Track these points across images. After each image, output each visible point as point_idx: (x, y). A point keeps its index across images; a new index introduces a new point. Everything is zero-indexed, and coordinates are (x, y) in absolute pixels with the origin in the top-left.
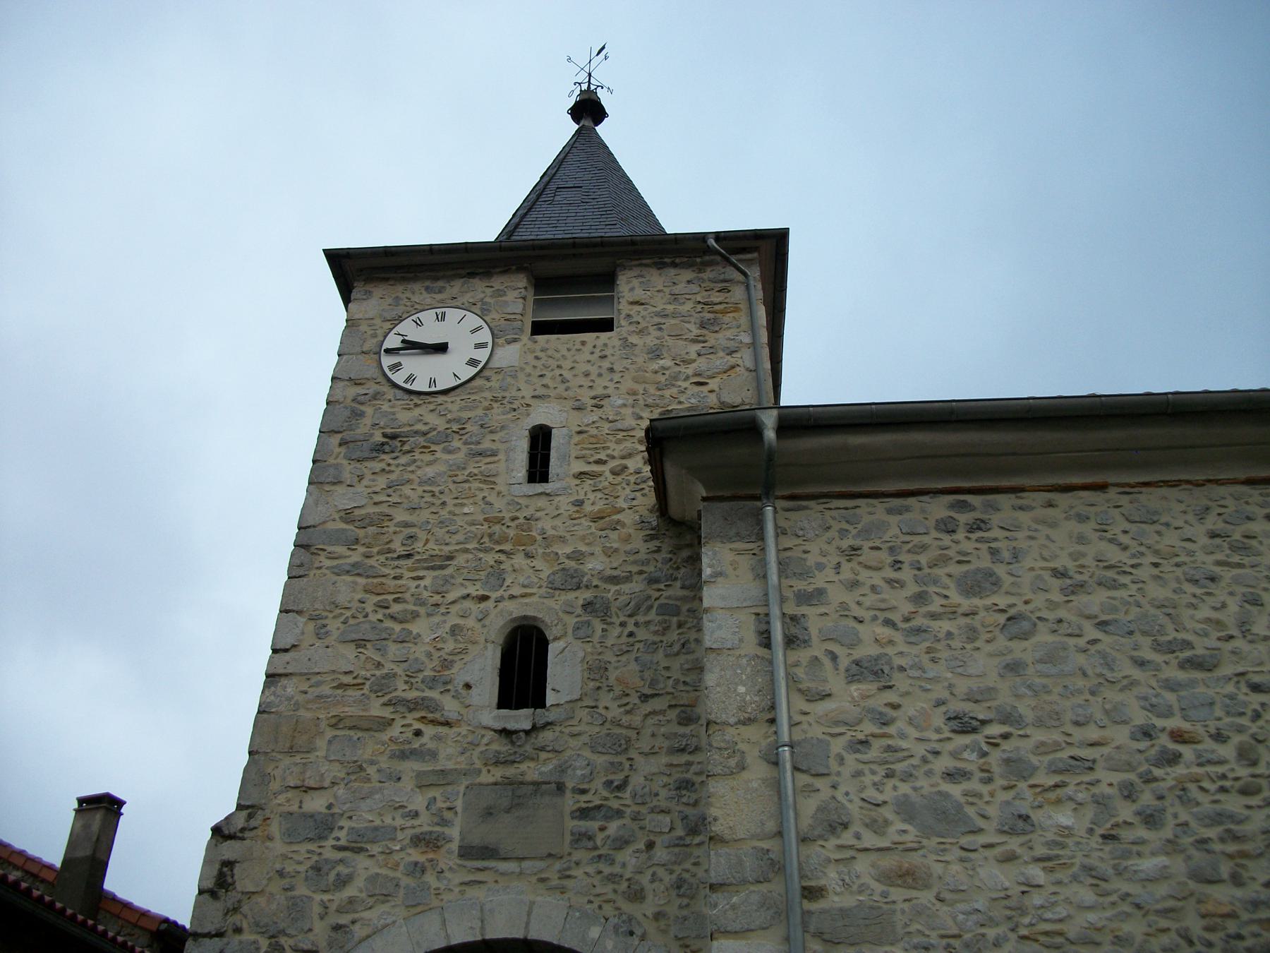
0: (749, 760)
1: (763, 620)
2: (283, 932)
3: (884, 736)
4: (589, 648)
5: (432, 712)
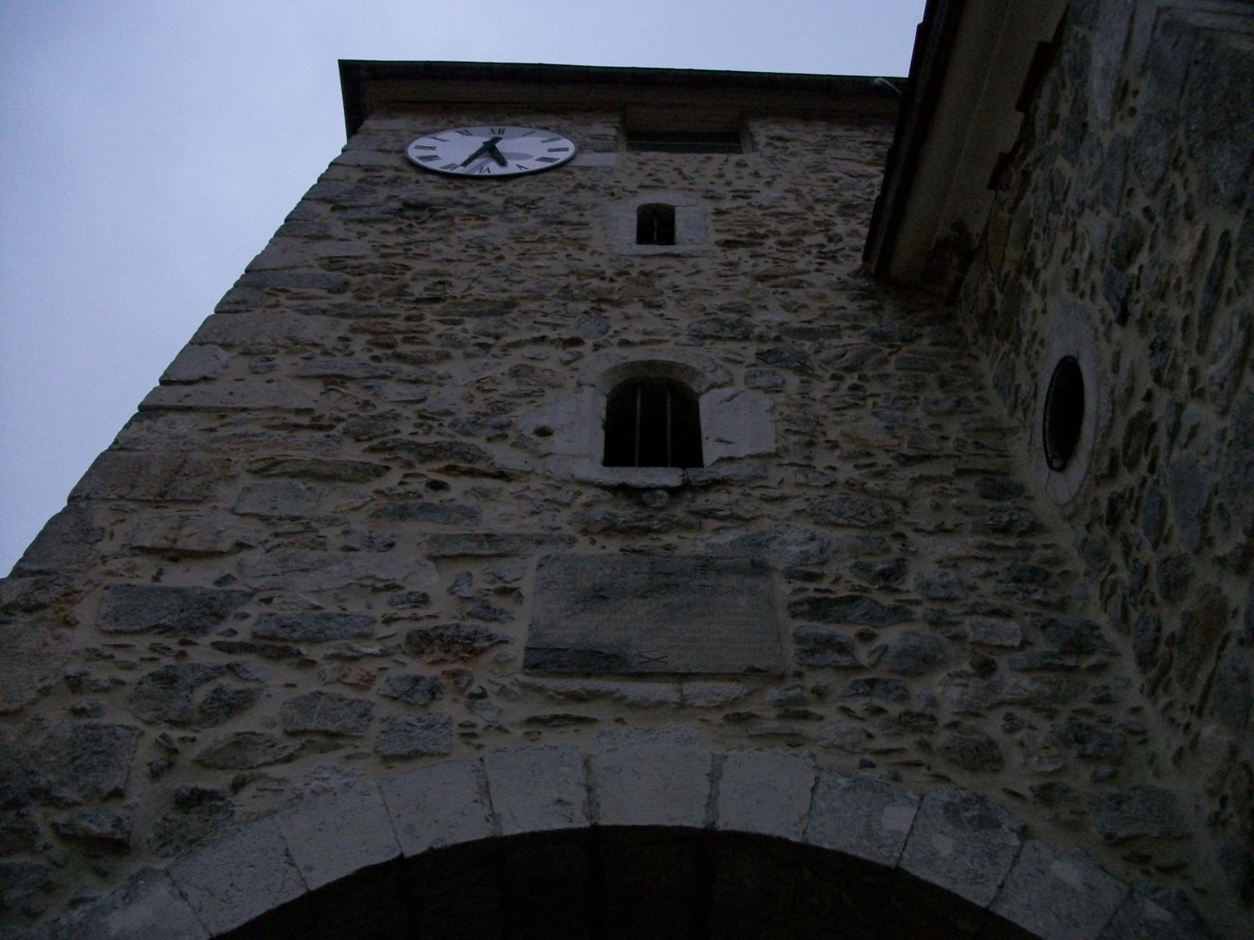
5: (470, 462)
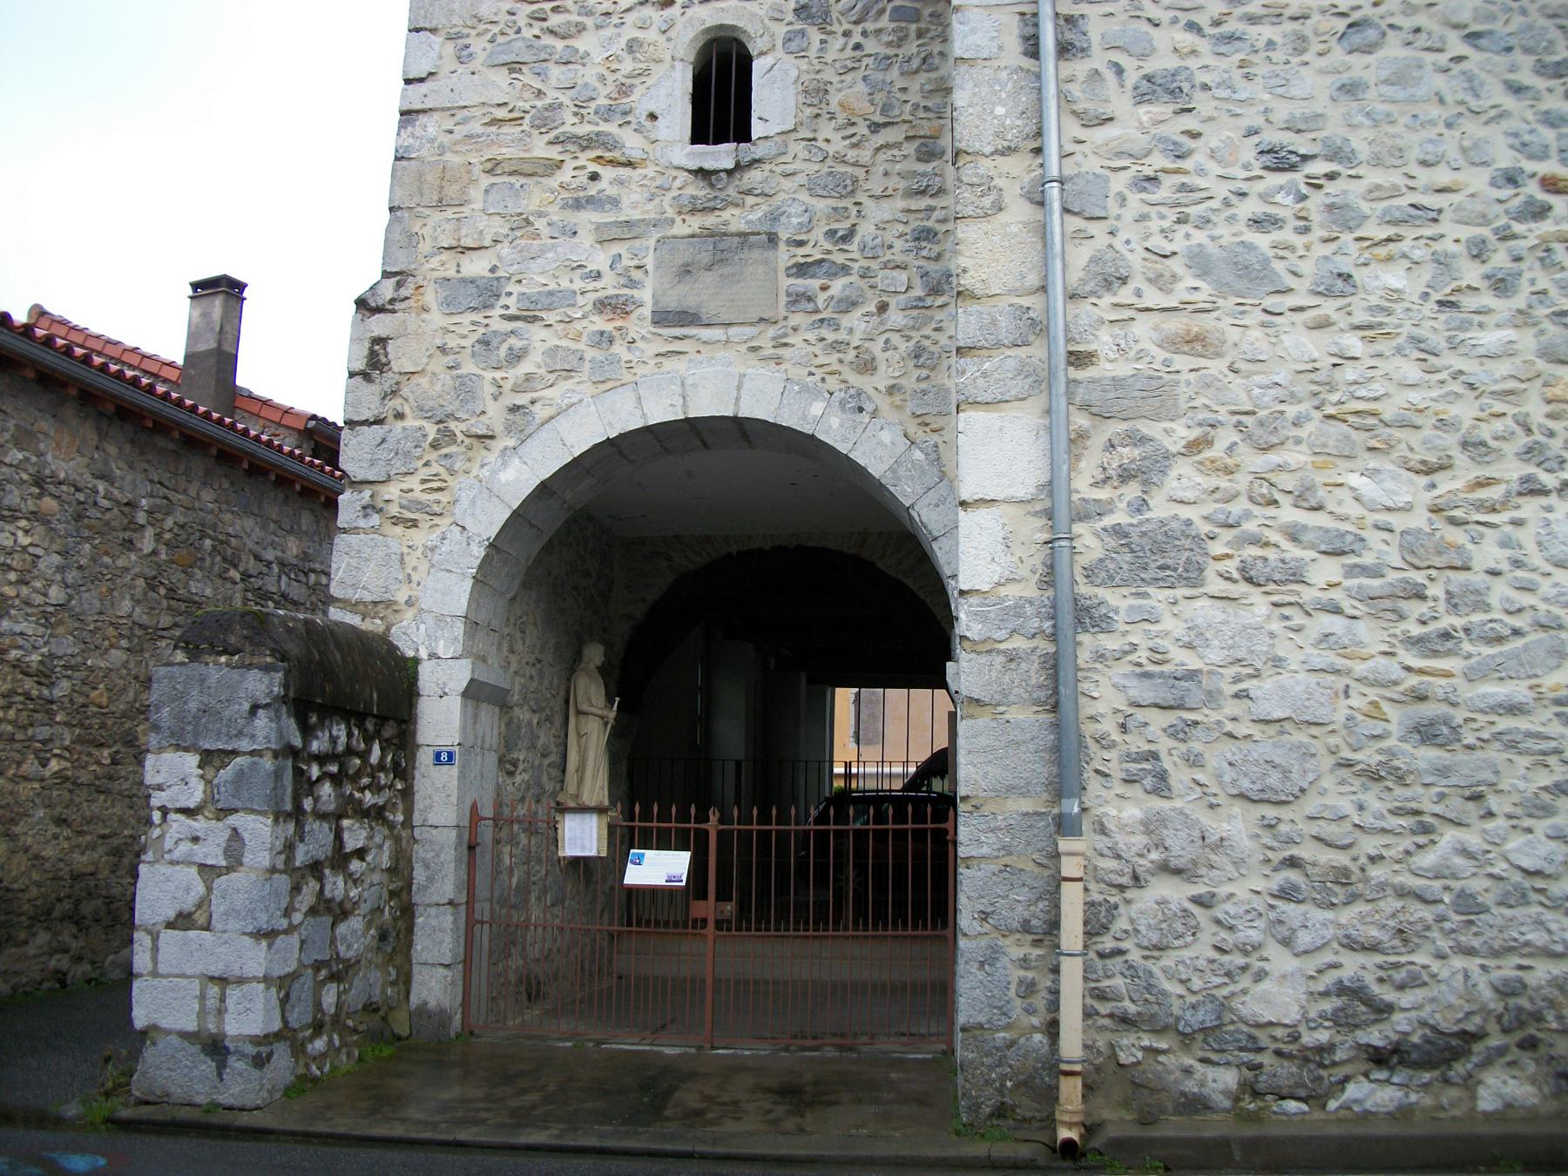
0: (1007, 199)
1: (1031, 21)
2: (451, 415)
3: (1177, 171)
4: (803, 64)
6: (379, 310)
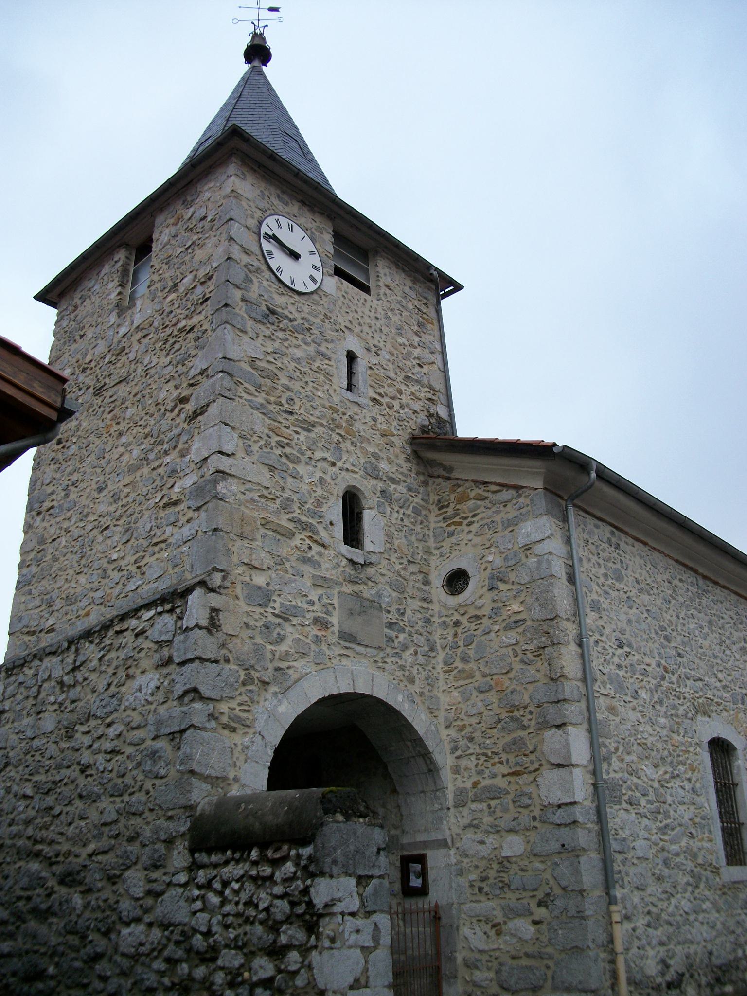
6: (212, 590)
